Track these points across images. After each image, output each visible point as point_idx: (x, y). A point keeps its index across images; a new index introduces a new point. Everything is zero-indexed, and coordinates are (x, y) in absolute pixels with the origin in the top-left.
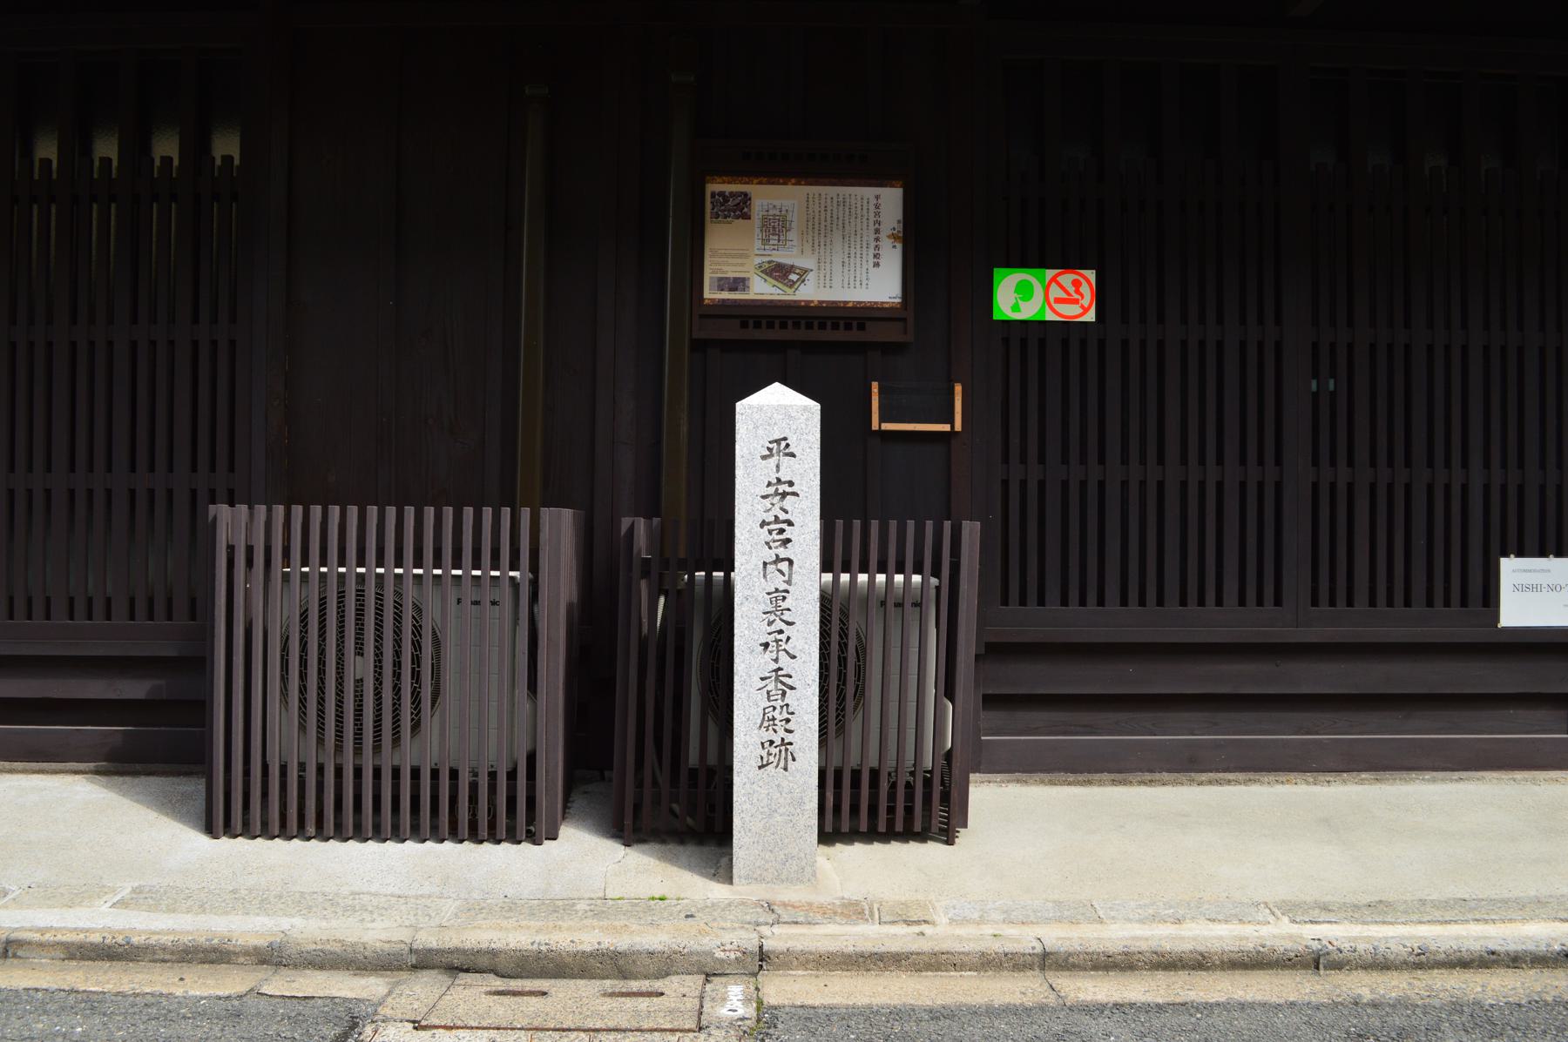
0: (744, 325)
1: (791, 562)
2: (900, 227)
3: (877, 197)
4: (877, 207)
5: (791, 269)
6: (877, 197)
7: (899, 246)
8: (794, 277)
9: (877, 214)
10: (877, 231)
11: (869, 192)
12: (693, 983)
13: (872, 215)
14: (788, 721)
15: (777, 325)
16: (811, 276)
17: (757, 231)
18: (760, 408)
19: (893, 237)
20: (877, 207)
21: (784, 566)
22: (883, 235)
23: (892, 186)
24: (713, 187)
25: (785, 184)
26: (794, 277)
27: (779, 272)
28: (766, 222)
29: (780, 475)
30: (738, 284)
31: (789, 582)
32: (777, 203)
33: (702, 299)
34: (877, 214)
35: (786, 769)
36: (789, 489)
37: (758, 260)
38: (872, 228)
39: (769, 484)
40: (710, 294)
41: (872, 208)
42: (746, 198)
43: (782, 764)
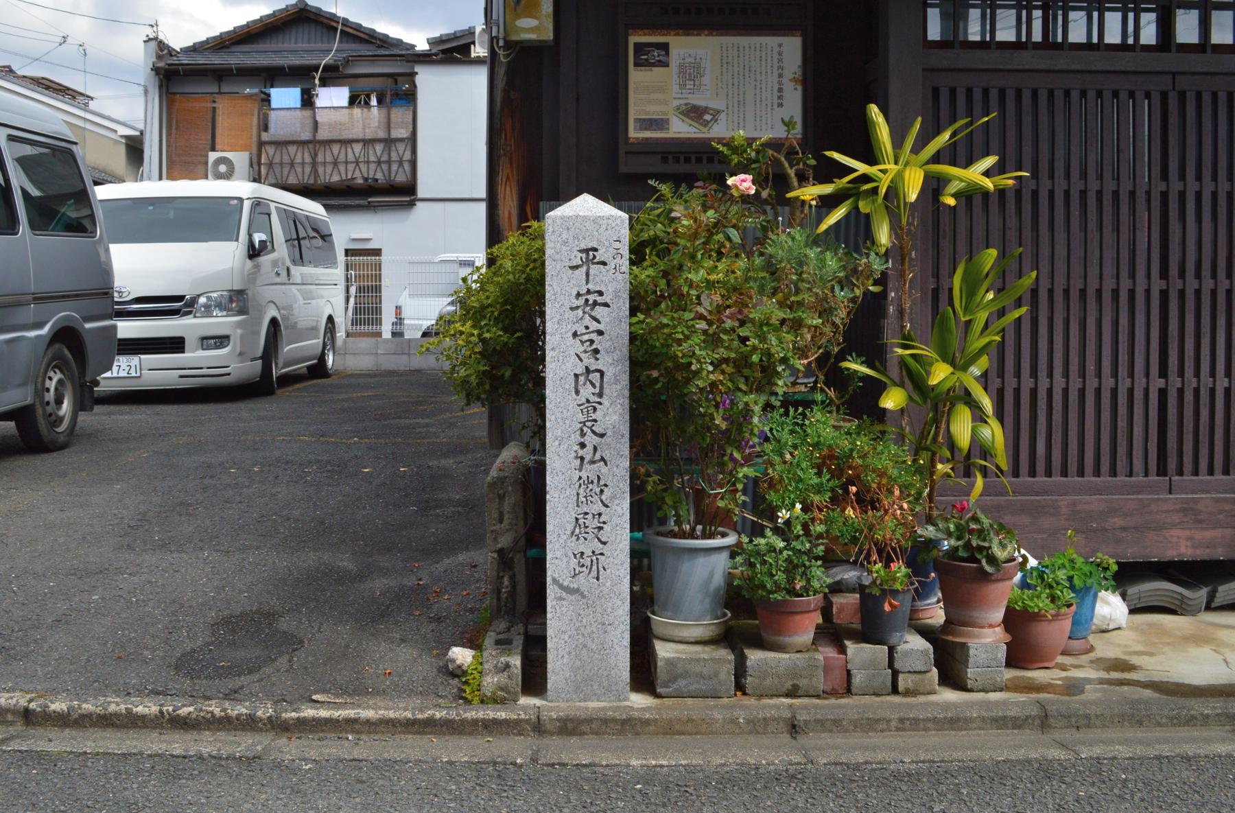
0: (665, 160)
1: (602, 373)
2: (799, 72)
3: (780, 46)
4: (780, 54)
5: (706, 110)
6: (780, 46)
7: (800, 88)
8: (708, 117)
9: (780, 60)
10: (780, 76)
11: (772, 41)
12: (901, 677)
13: (775, 61)
14: (600, 528)
15: (705, 160)
16: (723, 116)
17: (675, 77)
18: (562, 218)
19: (794, 80)
20: (780, 54)
21: (595, 377)
22: (785, 80)
23: (793, 35)
24: (634, 39)
25: (699, 35)
26: (708, 117)
27: (695, 113)
28: (682, 70)
29: (591, 286)
30: (660, 124)
31: (600, 395)
32: (692, 52)
33: (627, 138)
34: (780, 60)
35: (598, 579)
36: (599, 299)
37: (676, 103)
38: (776, 73)
39: (579, 295)
40: (634, 133)
41: (776, 57)
42: (665, 47)
43: (594, 573)
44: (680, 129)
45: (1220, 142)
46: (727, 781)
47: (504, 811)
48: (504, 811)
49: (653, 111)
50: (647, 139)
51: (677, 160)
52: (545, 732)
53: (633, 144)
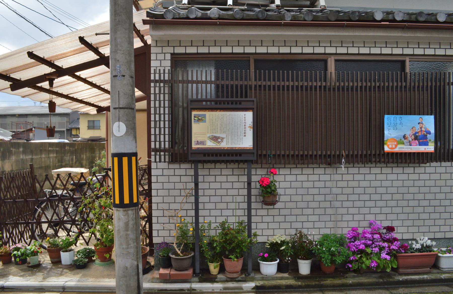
2: (252, 124)
3: (245, 115)
5: (219, 138)
6: (245, 115)
7: (252, 130)
8: (219, 140)
16: (225, 140)
19: (250, 127)
20: (245, 118)
26: (219, 140)
27: (215, 139)
30: (203, 143)
37: (208, 135)
40: (194, 146)
42: (204, 116)
44: (210, 144)
45: (448, 141)
46: (106, 292)
47: (230, 1)
48: (230, 1)
49: (200, 139)
50: (198, 148)
51: (224, 104)
52: (115, 17)
53: (193, 150)
